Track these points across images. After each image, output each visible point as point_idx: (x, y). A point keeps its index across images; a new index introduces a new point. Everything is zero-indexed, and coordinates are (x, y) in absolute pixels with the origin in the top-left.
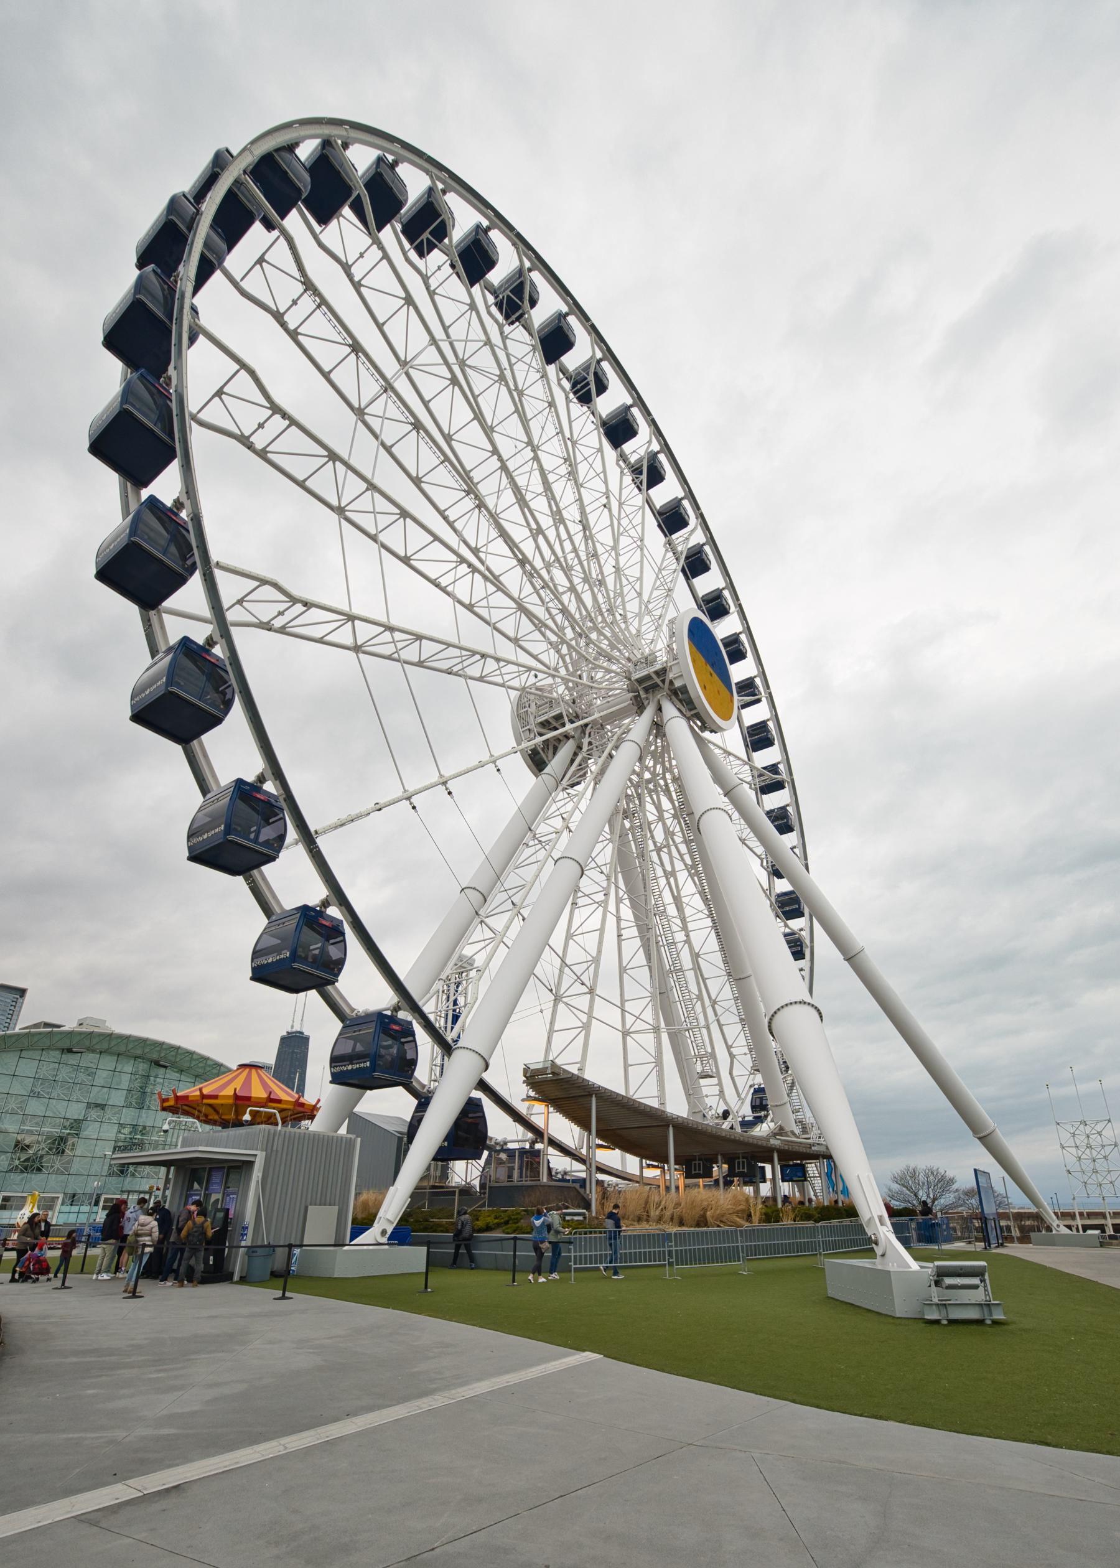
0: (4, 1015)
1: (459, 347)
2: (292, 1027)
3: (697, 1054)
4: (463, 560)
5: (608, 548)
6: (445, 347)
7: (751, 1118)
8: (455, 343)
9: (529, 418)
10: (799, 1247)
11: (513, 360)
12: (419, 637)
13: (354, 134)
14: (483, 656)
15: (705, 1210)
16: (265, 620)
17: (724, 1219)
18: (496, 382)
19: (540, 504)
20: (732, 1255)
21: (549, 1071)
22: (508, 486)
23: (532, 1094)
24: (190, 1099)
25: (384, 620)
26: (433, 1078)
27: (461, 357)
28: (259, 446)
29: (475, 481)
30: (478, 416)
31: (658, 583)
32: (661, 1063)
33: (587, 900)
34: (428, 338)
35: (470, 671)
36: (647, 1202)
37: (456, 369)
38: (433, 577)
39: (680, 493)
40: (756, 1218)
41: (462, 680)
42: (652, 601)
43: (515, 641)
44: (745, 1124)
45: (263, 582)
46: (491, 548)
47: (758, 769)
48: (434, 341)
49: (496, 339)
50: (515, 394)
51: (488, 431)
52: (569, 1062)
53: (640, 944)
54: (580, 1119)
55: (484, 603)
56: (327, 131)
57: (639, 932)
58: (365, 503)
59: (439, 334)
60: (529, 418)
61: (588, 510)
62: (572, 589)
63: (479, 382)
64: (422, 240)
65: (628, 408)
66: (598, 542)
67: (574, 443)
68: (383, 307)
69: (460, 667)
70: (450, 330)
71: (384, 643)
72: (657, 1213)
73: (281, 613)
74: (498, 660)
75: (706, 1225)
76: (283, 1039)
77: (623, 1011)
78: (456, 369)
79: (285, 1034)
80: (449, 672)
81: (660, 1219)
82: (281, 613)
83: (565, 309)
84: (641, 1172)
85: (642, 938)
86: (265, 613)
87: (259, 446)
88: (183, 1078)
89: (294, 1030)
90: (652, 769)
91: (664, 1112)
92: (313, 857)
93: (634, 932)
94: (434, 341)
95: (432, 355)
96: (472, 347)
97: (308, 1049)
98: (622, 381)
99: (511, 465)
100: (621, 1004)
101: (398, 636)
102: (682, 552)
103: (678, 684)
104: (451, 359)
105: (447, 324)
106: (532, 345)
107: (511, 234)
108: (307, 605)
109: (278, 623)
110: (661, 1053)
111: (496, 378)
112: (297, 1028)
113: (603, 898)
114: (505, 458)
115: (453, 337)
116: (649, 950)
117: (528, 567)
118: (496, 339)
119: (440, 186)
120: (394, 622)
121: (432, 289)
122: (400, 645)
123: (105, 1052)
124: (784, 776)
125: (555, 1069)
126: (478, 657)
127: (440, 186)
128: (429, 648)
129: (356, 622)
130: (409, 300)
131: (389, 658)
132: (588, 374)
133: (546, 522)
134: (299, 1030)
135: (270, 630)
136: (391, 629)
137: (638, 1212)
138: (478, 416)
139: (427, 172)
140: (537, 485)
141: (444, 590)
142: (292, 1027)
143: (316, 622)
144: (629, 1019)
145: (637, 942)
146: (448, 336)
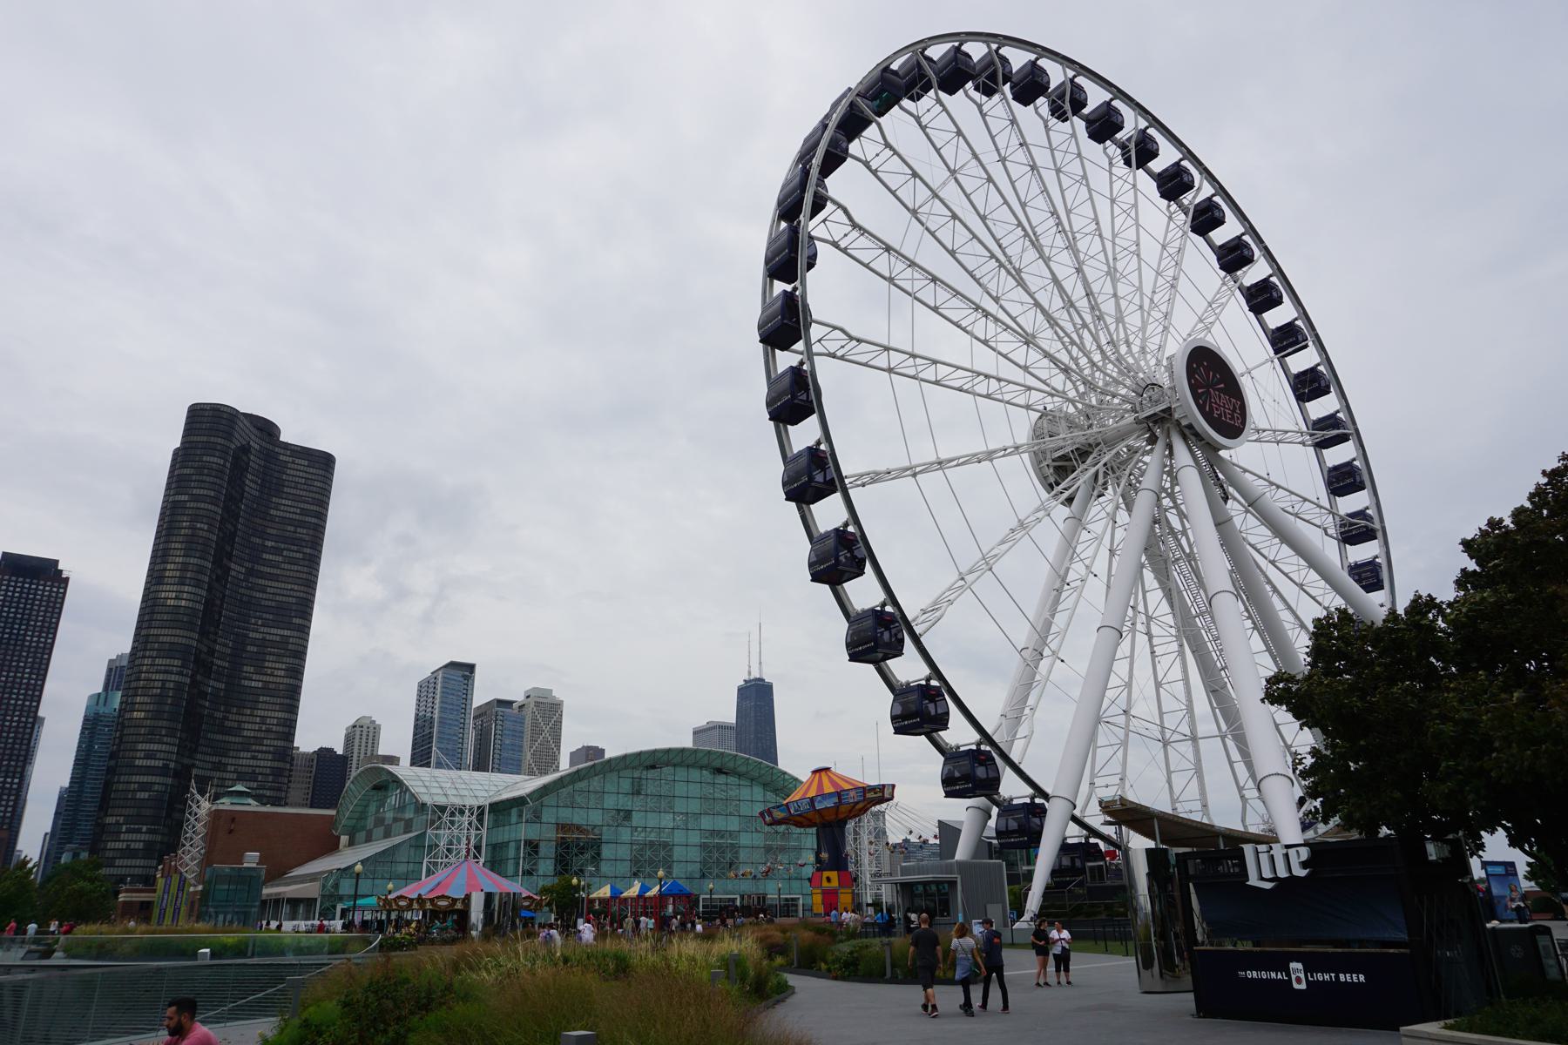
0: (460, 691)
2: (750, 673)
3: (1198, 611)
4: (993, 256)
12: (935, 362)
14: (987, 376)
16: (832, 351)
23: (1109, 819)
25: (910, 350)
28: (843, 246)
32: (1201, 768)
35: (978, 389)
38: (956, 320)
41: (971, 396)
42: (1157, 291)
43: (1025, 368)
45: (835, 328)
47: (1341, 517)
53: (1162, 595)
55: (994, 339)
56: (911, 49)
58: (918, 285)
65: (1108, 104)
69: (970, 385)
71: (909, 366)
73: (843, 347)
74: (999, 380)
76: (740, 690)
77: (1111, 174)
80: (960, 389)
82: (843, 347)
83: (1033, 57)
85: (1163, 589)
86: (832, 347)
87: (843, 246)
88: (741, 783)
89: (752, 677)
90: (1169, 490)
91: (1213, 826)
98: (1101, 86)
101: (919, 361)
102: (849, 945)
103: (1184, 423)
106: (1010, 120)
108: (859, 341)
109: (839, 354)
110: (1200, 760)
112: (755, 674)
113: (1136, 248)
116: (1171, 599)
120: (917, 352)
122: (920, 369)
124: (1377, 526)
126: (982, 378)
128: (943, 371)
129: (891, 352)
131: (913, 377)
132: (1064, 102)
135: (834, 357)
136: (914, 356)
141: (964, 329)
142: (750, 673)
143: (863, 352)
145: (1160, 593)
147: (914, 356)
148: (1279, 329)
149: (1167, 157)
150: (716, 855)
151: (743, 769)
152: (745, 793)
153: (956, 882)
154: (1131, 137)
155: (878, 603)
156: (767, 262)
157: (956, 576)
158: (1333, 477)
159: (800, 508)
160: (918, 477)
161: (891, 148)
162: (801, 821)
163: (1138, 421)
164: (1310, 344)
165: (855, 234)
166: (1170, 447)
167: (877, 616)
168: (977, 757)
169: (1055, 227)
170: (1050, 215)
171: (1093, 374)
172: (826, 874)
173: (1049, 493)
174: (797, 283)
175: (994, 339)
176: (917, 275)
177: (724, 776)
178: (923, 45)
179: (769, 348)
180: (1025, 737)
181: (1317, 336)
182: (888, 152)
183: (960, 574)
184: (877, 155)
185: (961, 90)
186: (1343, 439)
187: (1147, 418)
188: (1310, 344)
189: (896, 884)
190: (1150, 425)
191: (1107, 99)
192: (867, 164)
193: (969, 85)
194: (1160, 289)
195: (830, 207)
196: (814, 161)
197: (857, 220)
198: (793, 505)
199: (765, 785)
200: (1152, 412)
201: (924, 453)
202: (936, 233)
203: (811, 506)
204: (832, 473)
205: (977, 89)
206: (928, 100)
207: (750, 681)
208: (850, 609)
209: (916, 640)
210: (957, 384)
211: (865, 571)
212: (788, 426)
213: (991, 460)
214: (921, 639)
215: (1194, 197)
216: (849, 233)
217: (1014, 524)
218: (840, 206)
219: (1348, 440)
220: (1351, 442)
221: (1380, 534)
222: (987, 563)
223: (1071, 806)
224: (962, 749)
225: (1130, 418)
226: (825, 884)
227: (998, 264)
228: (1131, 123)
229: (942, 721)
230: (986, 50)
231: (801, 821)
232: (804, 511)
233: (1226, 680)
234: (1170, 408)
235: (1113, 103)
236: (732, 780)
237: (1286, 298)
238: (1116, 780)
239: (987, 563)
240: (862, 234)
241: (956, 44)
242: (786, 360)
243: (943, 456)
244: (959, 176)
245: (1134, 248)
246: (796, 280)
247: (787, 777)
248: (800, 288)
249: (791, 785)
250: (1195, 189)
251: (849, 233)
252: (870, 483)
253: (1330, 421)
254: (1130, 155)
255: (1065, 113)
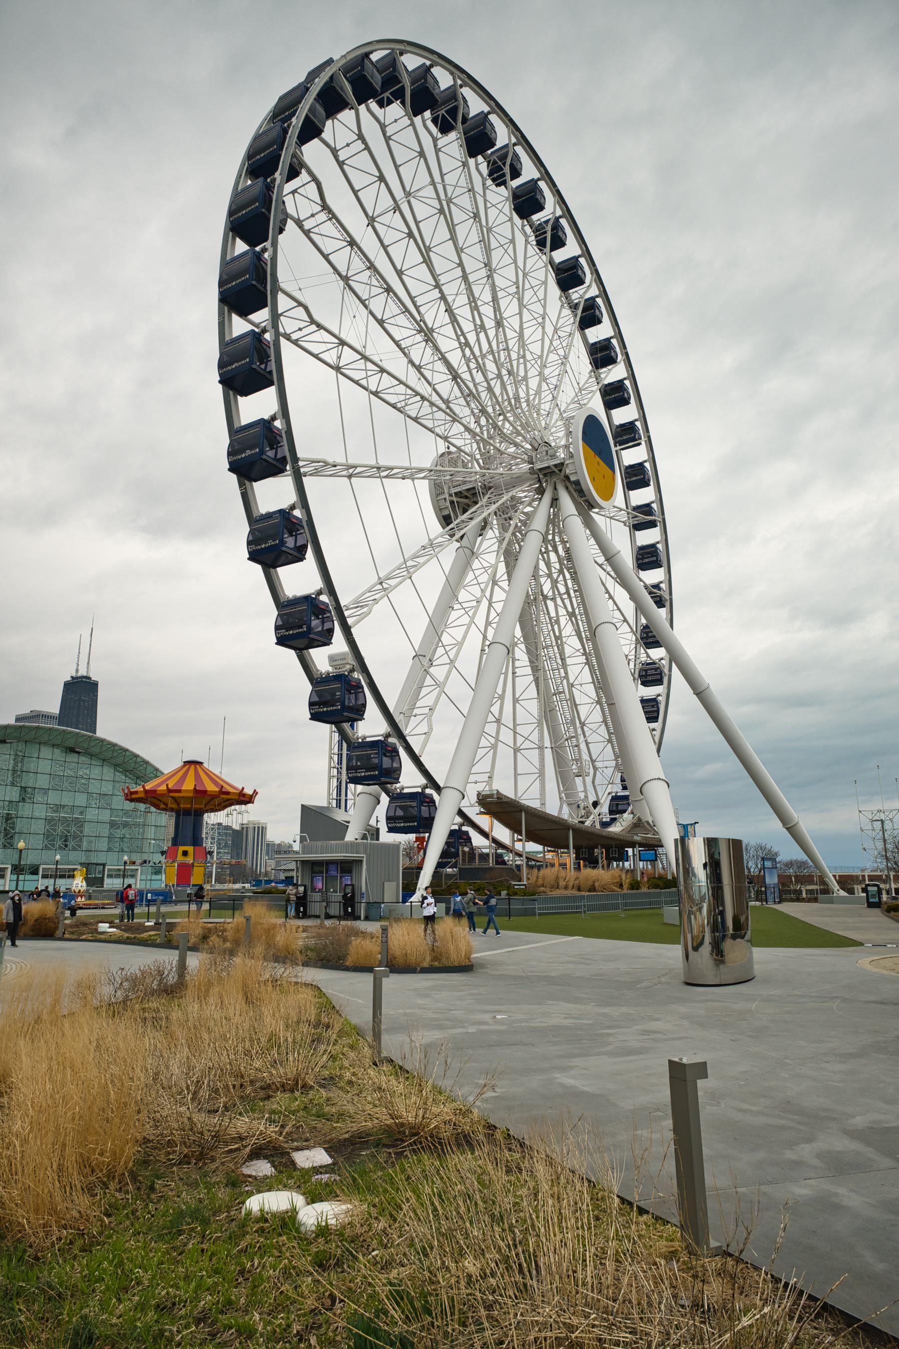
1: (450, 190)
2: (77, 671)
5: (535, 357)
6: (440, 188)
7: (608, 820)
8: (447, 187)
9: (492, 248)
10: (651, 903)
11: (489, 205)
13: (409, 48)
15: (594, 882)
17: (606, 887)
18: (472, 218)
19: (487, 311)
20: (615, 907)
21: (495, 796)
22: (465, 292)
23: (482, 810)
24: (158, 792)
26: (332, 765)
27: (449, 196)
28: (306, 227)
29: (441, 282)
30: (453, 238)
31: (552, 348)
33: (458, 606)
34: (429, 180)
36: (557, 878)
37: (444, 203)
39: (578, 252)
40: (625, 887)
42: (548, 365)
44: (605, 825)
46: (442, 331)
48: (433, 183)
49: (478, 188)
50: (485, 230)
51: (459, 251)
52: (508, 791)
54: (514, 827)
55: (430, 367)
56: (392, 46)
57: (533, 672)
59: (437, 179)
60: (492, 248)
61: (525, 326)
62: (499, 376)
63: (458, 216)
64: (439, 115)
66: (529, 350)
67: (525, 275)
68: (401, 155)
70: (446, 177)
72: (564, 883)
73: (300, 329)
75: (595, 890)
76: (67, 685)
77: (515, 733)
78: (444, 203)
79: (69, 679)
81: (566, 888)
82: (300, 329)
84: (514, 845)
87: (306, 227)
88: (93, 762)
89: (80, 674)
92: (349, 643)
93: (529, 670)
94: (433, 183)
95: (430, 192)
96: (458, 191)
97: (97, 696)
99: (471, 278)
100: (514, 727)
103: (573, 478)
104: (442, 196)
105: (444, 172)
107: (505, 119)
108: (320, 327)
109: (294, 337)
111: (472, 215)
112: (82, 672)
114: (468, 272)
115: (447, 182)
117: (468, 352)
118: (478, 188)
119: (459, 82)
121: (438, 147)
123: (30, 742)
125: (499, 796)
126: (418, 398)
127: (459, 82)
130: (422, 154)
132: (504, 164)
133: (490, 324)
134: (85, 674)
136: (365, 358)
137: (552, 883)
138: (453, 238)
139: (452, 73)
140: (487, 296)
142: (77, 671)
144: (520, 740)
146: (443, 180)
147: (365, 358)
148: (622, 426)
149: (570, 250)
150: (74, 828)
151: (96, 750)
152: (96, 772)
153: (361, 861)
154: (549, 220)
155: (313, 591)
156: (231, 213)
157: (376, 579)
158: (640, 554)
159: (241, 484)
160: (353, 479)
161: (364, 141)
162: (153, 799)
163: (532, 471)
164: (643, 443)
165: (323, 216)
166: (555, 501)
167: (309, 602)
168: (382, 747)
169: (486, 278)
170: (483, 265)
171: (503, 424)
172: (181, 849)
173: (444, 528)
174: (268, 244)
175: (430, 367)
176: (374, 282)
177: (76, 755)
178: (401, 47)
179: (226, 308)
180: (425, 734)
181: (649, 437)
182: (359, 145)
183: (379, 578)
184: (348, 145)
185: (420, 116)
186: (652, 524)
187: (540, 470)
188: (643, 443)
189: (297, 861)
190: (541, 476)
191: (536, 178)
192: (334, 152)
193: (427, 114)
194: (550, 365)
195: (304, 176)
196: (294, 120)
197: (329, 201)
198: (234, 477)
199: (116, 766)
200: (547, 465)
201: (362, 456)
202: (389, 248)
203: (254, 483)
204: (285, 451)
205: (435, 121)
206: (395, 110)
207: (77, 678)
208: (281, 595)
209: (347, 631)
210: (392, 399)
211: (306, 556)
212: (238, 396)
213: (413, 480)
214: (352, 630)
215: (585, 293)
216: (317, 214)
217: (425, 541)
218: (315, 179)
219: (655, 526)
220: (658, 528)
221: (668, 604)
222: (409, 572)
223: (461, 796)
224: (368, 739)
225: (525, 467)
226: (180, 858)
227: (440, 295)
228: (550, 210)
229: (358, 712)
230: (452, 83)
231: (153, 799)
232: (245, 488)
233: (556, 703)
234: (562, 464)
235: (539, 183)
236: (83, 759)
237: (632, 400)
238: (485, 777)
239: (409, 572)
240: (330, 219)
241: (428, 63)
242: (239, 326)
243: (382, 463)
244: (412, 200)
245: (540, 320)
246: (266, 240)
247: (139, 760)
248: (271, 250)
249: (141, 768)
250: (585, 285)
251: (317, 214)
252: (311, 475)
253: (646, 509)
254: (546, 238)
255: (504, 175)
